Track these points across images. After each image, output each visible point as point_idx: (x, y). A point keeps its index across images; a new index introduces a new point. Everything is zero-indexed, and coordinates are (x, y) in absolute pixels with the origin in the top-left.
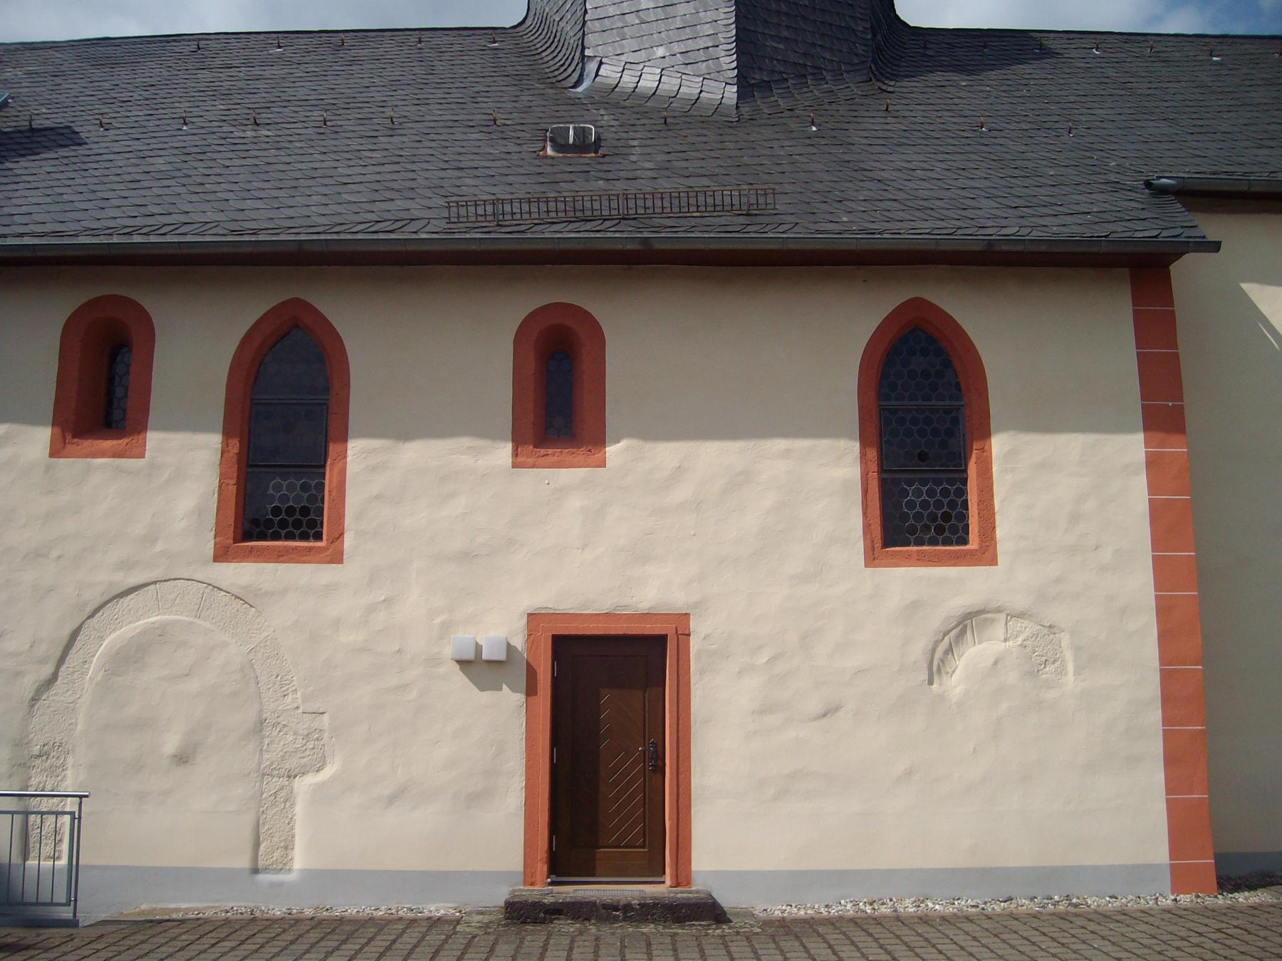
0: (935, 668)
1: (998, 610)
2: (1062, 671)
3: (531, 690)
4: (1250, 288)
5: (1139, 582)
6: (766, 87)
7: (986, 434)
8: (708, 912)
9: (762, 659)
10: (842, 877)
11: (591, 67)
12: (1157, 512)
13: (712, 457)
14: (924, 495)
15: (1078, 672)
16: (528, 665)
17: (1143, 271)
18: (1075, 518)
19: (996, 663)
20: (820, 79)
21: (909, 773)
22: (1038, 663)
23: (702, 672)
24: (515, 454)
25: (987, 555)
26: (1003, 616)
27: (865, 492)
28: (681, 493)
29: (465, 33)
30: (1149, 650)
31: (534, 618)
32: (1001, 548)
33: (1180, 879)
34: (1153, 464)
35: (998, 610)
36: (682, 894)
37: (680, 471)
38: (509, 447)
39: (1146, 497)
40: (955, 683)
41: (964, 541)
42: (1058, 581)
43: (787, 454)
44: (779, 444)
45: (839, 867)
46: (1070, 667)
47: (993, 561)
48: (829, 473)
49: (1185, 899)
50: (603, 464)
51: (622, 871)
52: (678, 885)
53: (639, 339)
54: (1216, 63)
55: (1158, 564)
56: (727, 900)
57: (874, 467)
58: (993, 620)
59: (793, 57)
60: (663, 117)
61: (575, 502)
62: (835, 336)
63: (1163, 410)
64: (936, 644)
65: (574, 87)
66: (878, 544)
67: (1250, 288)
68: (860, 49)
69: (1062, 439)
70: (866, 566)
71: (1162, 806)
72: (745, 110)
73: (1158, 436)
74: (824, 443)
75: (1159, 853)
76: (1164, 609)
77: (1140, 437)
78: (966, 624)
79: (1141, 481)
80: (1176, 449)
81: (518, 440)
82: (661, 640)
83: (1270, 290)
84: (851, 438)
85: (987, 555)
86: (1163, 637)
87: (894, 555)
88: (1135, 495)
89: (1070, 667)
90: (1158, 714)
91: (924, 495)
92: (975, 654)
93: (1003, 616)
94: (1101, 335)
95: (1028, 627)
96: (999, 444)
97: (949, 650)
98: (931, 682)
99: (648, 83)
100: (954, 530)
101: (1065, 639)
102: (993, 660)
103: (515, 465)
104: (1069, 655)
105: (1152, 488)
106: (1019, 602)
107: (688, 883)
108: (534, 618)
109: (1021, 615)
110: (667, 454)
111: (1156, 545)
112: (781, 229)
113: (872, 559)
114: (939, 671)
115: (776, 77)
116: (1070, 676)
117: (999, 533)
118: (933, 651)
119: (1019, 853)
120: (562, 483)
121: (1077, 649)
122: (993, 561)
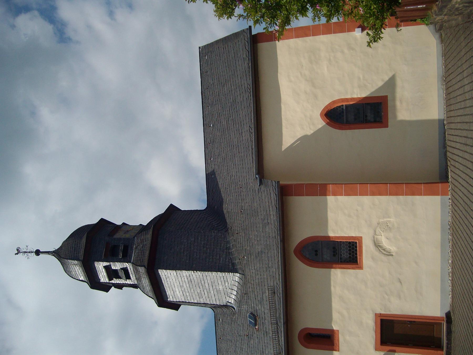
0: (389, 254)
1: (374, 237)
2: (389, 221)
3: (395, 351)
4: (284, 147)
5: (366, 200)
6: (233, 264)
7: (329, 237)
8: (448, 315)
9: (386, 296)
10: (442, 281)
11: (229, 304)
12: (347, 194)
13: (336, 305)
14: (346, 253)
15: (389, 217)
16: (388, 351)
17: (284, 192)
18: (350, 216)
19: (388, 239)
20: (229, 248)
21: (416, 263)
22: (388, 228)
23: (390, 311)
24: (336, 350)
25: (360, 239)
26: (375, 236)
27: (344, 268)
28: (345, 313)
29: (217, 325)
30: (384, 199)
31: (376, 349)
32: (358, 235)
33: (444, 193)
34: (335, 194)
35: (374, 237)
36: (445, 320)
37: (339, 313)
38: (334, 352)
39: (343, 197)
40: (393, 249)
41: (356, 242)
42: (366, 221)
43: (334, 287)
44: (332, 288)
45: (440, 281)
46: (389, 219)
47: (361, 237)
48: (339, 277)
49: (449, 193)
50: (338, 331)
51: (440, 331)
52: (444, 320)
53: (308, 320)
54: (213, 125)
55: (361, 195)
56: (447, 309)
57: (337, 266)
58: (377, 238)
59: (224, 256)
60: (244, 293)
61: (348, 338)
62: (304, 273)
63: (321, 190)
64: (384, 254)
65: (235, 309)
66: (357, 266)
67: (284, 147)
68: (220, 234)
69: (329, 218)
70: (363, 269)
71: (425, 197)
72: (240, 272)
73: (328, 192)
74: (332, 278)
75: (437, 199)
76: (373, 194)
77: (328, 197)
78: (377, 245)
79: (339, 197)
80: (331, 187)
81: (333, 350)
82: (382, 320)
83: (283, 143)
84: (330, 271)
85: (360, 239)
86: (380, 194)
87: (360, 262)
88: (343, 199)
89: (389, 219)
90: (401, 197)
91: (346, 253)
92: (385, 243)
93: (375, 236)
94: (302, 205)
95: (378, 230)
96: (331, 234)
97: (384, 250)
98: (392, 255)
99: (235, 293)
100: (353, 245)
101: (381, 220)
102: (387, 240)
103: (339, 351)
104: (385, 220)
105: (341, 195)
106: (372, 232)
107: (443, 317)
108: (376, 349)
109: (375, 231)
110: (335, 316)
111: (356, 195)
112: (278, 283)
113: (361, 268)
114: (389, 253)
115: (230, 261)
116: (391, 219)
117: (354, 235)
118: (384, 254)
119: (437, 235)
120: (343, 340)
121: (384, 217)
122: (361, 237)
